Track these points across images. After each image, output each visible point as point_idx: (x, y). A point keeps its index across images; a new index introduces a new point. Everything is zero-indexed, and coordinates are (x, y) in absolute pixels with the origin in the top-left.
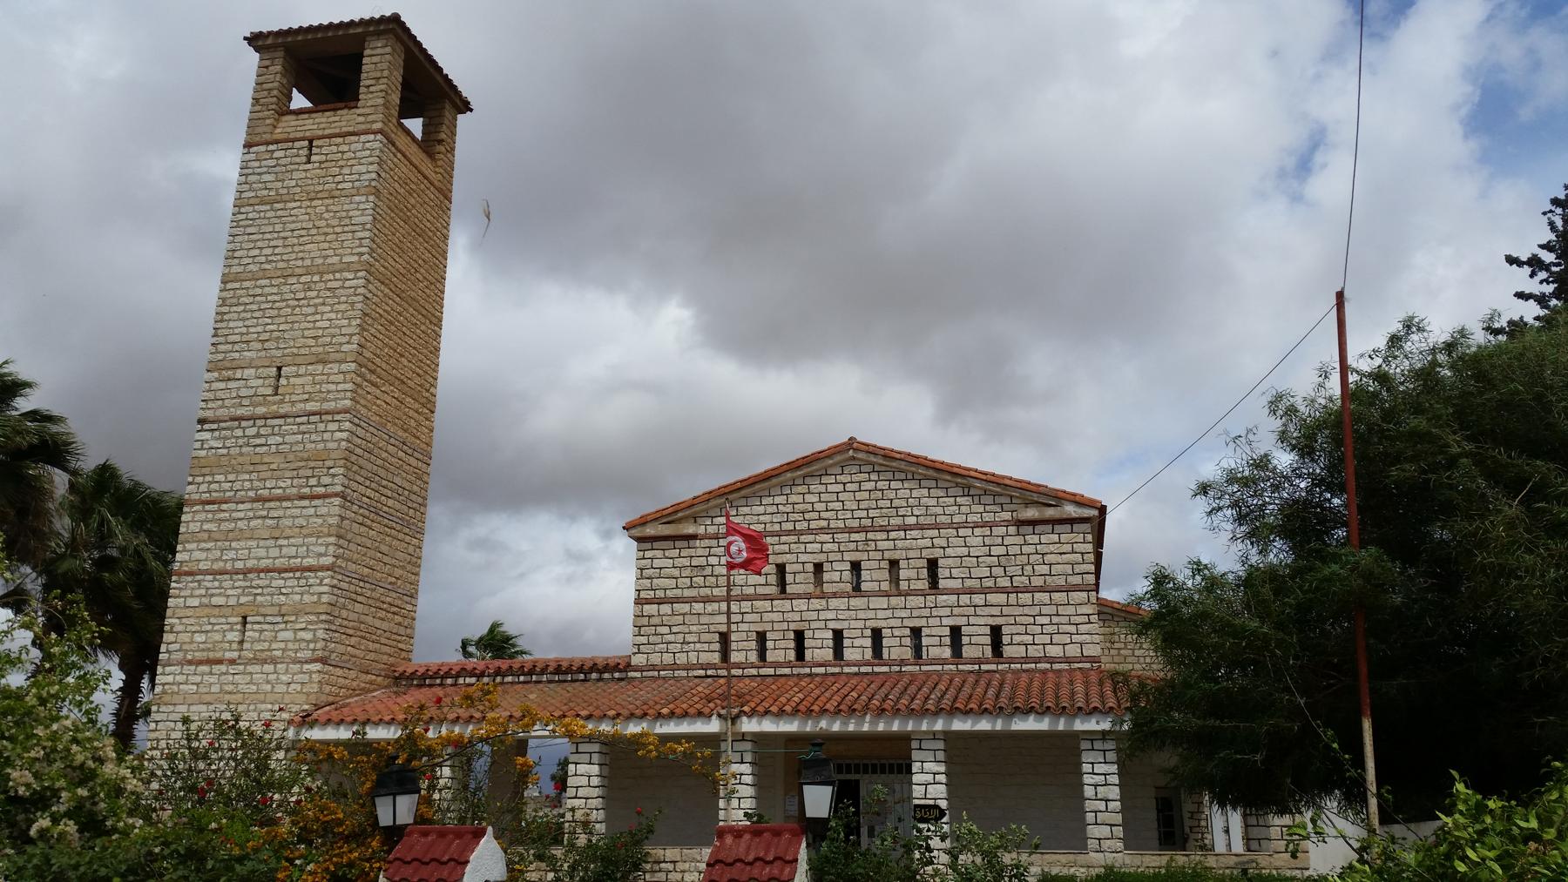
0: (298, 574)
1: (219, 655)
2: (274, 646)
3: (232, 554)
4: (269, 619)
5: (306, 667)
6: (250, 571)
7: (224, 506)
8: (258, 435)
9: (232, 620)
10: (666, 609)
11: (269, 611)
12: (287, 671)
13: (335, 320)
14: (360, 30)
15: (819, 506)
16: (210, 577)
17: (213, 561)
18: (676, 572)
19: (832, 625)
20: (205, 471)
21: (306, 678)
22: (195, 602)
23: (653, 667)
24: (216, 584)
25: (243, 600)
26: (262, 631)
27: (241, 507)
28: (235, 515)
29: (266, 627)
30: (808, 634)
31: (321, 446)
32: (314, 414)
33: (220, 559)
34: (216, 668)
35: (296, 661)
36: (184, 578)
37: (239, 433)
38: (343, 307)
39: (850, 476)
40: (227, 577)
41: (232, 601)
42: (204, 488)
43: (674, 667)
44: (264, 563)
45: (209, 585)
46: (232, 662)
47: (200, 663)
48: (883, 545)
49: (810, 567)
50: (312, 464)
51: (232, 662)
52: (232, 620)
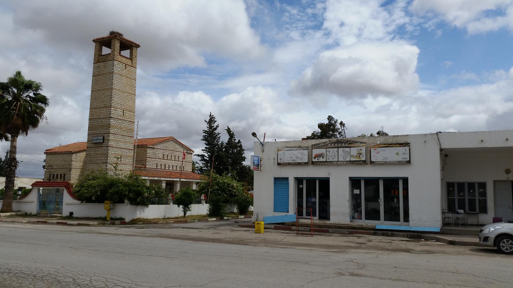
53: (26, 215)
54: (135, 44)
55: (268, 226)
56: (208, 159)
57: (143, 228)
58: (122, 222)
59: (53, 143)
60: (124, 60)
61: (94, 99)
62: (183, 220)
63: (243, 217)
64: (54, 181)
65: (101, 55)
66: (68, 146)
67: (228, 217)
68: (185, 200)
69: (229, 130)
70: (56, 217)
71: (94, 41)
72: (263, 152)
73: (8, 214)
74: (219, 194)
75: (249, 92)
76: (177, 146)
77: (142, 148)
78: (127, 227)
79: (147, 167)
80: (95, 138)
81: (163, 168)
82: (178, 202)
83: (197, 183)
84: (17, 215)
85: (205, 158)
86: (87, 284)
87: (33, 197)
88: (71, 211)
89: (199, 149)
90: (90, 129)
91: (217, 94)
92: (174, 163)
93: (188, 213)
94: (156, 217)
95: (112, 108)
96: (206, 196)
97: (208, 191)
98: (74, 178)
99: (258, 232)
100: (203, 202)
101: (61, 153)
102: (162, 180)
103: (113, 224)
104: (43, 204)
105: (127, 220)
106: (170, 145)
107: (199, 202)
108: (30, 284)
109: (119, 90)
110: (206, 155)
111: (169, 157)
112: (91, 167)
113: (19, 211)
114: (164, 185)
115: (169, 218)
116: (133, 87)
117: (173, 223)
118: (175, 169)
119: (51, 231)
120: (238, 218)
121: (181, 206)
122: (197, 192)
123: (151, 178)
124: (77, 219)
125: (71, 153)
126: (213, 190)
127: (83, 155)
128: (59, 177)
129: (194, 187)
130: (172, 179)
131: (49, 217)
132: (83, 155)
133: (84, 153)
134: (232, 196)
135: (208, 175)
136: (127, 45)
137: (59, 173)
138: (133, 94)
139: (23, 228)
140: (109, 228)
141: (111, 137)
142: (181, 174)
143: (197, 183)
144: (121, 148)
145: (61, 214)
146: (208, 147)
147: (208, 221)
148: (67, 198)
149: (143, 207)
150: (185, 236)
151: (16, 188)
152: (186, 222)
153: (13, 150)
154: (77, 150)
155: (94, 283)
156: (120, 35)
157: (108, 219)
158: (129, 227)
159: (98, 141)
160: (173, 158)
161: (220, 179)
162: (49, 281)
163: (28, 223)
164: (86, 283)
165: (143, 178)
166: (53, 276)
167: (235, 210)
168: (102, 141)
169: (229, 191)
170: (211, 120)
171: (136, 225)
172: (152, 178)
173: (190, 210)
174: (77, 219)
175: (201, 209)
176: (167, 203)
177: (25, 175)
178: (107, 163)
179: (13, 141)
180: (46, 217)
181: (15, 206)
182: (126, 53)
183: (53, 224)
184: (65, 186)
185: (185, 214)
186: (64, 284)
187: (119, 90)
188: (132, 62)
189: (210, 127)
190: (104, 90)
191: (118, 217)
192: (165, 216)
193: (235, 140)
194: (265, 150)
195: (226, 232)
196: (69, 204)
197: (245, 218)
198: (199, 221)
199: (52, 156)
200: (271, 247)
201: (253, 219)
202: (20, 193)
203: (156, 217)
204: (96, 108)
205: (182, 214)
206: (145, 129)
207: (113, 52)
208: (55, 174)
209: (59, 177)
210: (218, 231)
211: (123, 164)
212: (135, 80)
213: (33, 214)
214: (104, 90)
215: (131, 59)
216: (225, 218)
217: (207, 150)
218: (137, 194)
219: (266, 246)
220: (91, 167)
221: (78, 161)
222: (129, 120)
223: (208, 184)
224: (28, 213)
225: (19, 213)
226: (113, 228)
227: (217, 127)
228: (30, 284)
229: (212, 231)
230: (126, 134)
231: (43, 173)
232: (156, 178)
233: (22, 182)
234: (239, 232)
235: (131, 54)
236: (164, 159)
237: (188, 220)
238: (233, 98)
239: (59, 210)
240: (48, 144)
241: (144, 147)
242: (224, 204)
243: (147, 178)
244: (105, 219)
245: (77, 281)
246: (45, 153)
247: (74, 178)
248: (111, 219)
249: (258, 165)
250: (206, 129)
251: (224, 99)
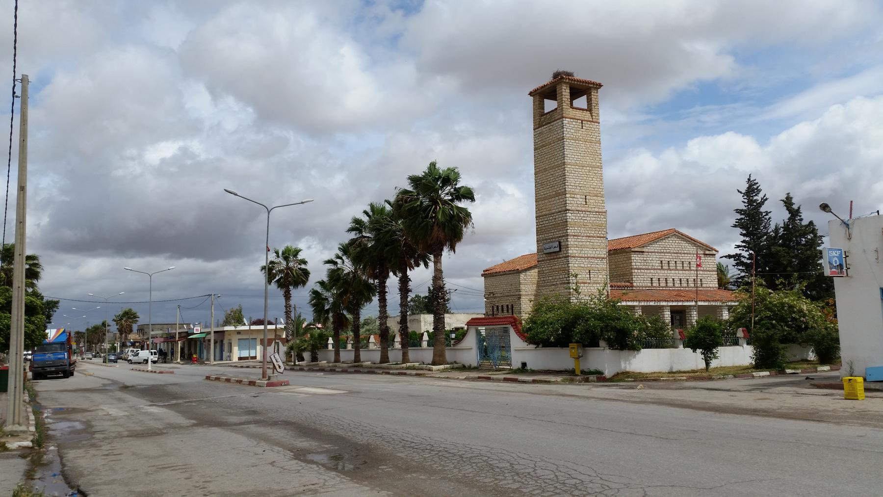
53: (464, 368)
54: (593, 83)
55: (872, 386)
56: (749, 261)
57: (632, 388)
58: (600, 377)
59: (494, 258)
60: (579, 114)
61: (540, 184)
62: (704, 374)
63: (826, 368)
64: (499, 315)
65: (543, 114)
66: (512, 262)
67: (794, 368)
68: (706, 340)
69: (788, 202)
70: (504, 369)
71: (531, 94)
72: (850, 239)
73: (442, 367)
74: (774, 326)
75: (834, 117)
76: (684, 244)
77: (620, 256)
78: (606, 386)
79: (635, 284)
80: (547, 246)
82: (693, 343)
83: (730, 308)
84: (453, 369)
85: (743, 259)
86: (529, 473)
87: (470, 341)
88: (524, 361)
89: (730, 244)
90: (539, 232)
91: (763, 134)
92: (683, 275)
93: (714, 364)
94: (657, 370)
96: (748, 329)
97: (750, 321)
98: (526, 308)
99: (852, 396)
100: (742, 341)
101: (504, 273)
102: (663, 306)
103: (587, 380)
104: (485, 352)
105: (608, 374)
106: (672, 244)
107: (736, 343)
108: (455, 468)
110: (746, 254)
111: (672, 264)
112: (545, 291)
113: (455, 362)
114: (667, 315)
115: (680, 372)
116: (597, 154)
117: (686, 380)
118: (685, 285)
119: (495, 390)
120: (816, 371)
121: (699, 351)
122: (731, 324)
124: (533, 372)
125: (518, 272)
126: (761, 319)
127: (534, 273)
128: (505, 308)
129: (726, 315)
130: (680, 304)
131: (493, 371)
132: (534, 273)
133: (536, 270)
134: (799, 329)
135: (747, 290)
136: (581, 89)
137: (505, 304)
139: (460, 386)
140: (579, 387)
141: (571, 241)
142: (697, 293)
143: (730, 308)
145: (510, 365)
146: (747, 239)
147: (753, 377)
148: (516, 341)
150: (702, 403)
151: (447, 328)
152: (710, 379)
153: (438, 276)
154: (526, 266)
155: (539, 472)
156: (569, 74)
157: (578, 372)
158: (609, 386)
159: (552, 250)
160: (679, 266)
161: (775, 297)
162: (479, 465)
163: (466, 379)
164: (527, 471)
165: (624, 303)
166: (485, 458)
167: (812, 356)
168: (557, 249)
169: (794, 319)
170: (752, 189)
171: (622, 384)
173: (716, 358)
174: (533, 372)
175: (741, 355)
176: (674, 346)
177: (462, 309)
179: (437, 262)
180: (489, 370)
181: (449, 355)
182: (581, 102)
183: (498, 380)
184: (511, 323)
185: (707, 364)
186: (498, 470)
189: (750, 202)
190: (553, 168)
191: (592, 369)
192: (671, 368)
193: (801, 220)
194: (853, 236)
195: (785, 397)
196: (519, 351)
197: (832, 370)
198: (735, 377)
199: (493, 279)
200: (875, 426)
201: (842, 372)
202: (453, 336)
203: (656, 369)
204: (545, 199)
205: (702, 365)
206: (625, 220)
207: (560, 105)
208: (500, 305)
209: (505, 308)
210: (767, 396)
211: (594, 283)
212: (599, 142)
213: (473, 366)
214: (553, 168)
215: (589, 110)
216: (788, 371)
217: (748, 246)
218: (617, 331)
219: (865, 425)
220: (545, 291)
221: (528, 283)
222: (596, 210)
223: (749, 309)
224: (467, 365)
225: (456, 365)
226: (584, 387)
228: (455, 468)
229: (757, 394)
230: (592, 233)
231: (484, 305)
232: (652, 304)
233: (454, 321)
234: (811, 397)
235: (589, 101)
236: (662, 269)
237: (714, 375)
238: (803, 133)
239: (507, 360)
240: (489, 260)
242: (783, 345)
243: (636, 304)
244: (572, 372)
245: (516, 467)
246: (482, 275)
247: (526, 308)
248: (583, 372)
249: (841, 266)
250: (742, 207)
251: (783, 136)
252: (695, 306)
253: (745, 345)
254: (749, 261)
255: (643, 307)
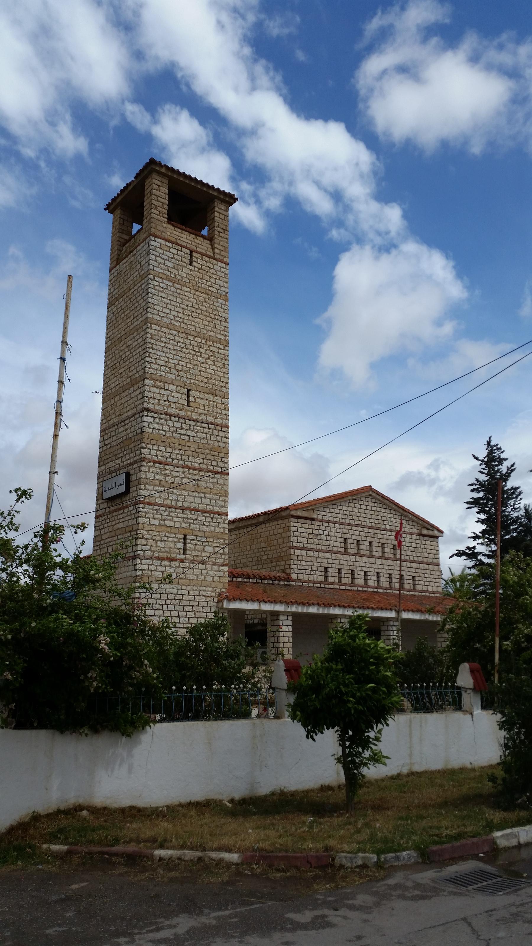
0: (212, 515)
1: (173, 556)
2: (204, 554)
3: (175, 497)
4: (199, 538)
5: (221, 568)
6: (186, 509)
7: (167, 467)
8: (181, 428)
9: (178, 536)
10: (304, 553)
11: (199, 534)
12: (212, 570)
13: (161, 356)
14: (215, 194)
15: (359, 514)
16: (164, 509)
17: (164, 499)
18: (307, 536)
19: (364, 569)
20: (153, 442)
21: (221, 574)
22: (156, 522)
23: (300, 581)
24: (167, 513)
25: (184, 525)
26: (196, 545)
27: (176, 469)
28: (173, 473)
29: (198, 543)
30: (356, 572)
31: (216, 444)
32: (212, 424)
33: (168, 498)
34: (173, 564)
35: (216, 564)
36: (147, 506)
37: (170, 423)
38: (219, 364)
39: (369, 502)
40: (173, 510)
41: (178, 525)
42: (153, 452)
43: (308, 581)
44: (193, 506)
45: (163, 513)
46: (182, 561)
47: (163, 559)
48: (380, 536)
49: (355, 542)
50: (214, 453)
51: (182, 561)
52: (178, 536)
79: (294, 576)
81: (346, 580)
95: (147, 381)
100: (470, 699)
109: (170, 327)
111: (365, 546)
118: (386, 584)
123: (293, 609)
138: (220, 341)
141: (148, 472)
144: (183, 509)
149: (102, 741)
172: (300, 609)
178: (135, 557)
187: (170, 327)
188: (212, 245)
189: (491, 474)
211: (192, 561)
222: (210, 419)
227: (511, 470)
232: (313, 610)
236: (346, 552)
241: (283, 518)
252: (396, 620)
253: (477, 711)
254: (491, 561)
255: (296, 618)
